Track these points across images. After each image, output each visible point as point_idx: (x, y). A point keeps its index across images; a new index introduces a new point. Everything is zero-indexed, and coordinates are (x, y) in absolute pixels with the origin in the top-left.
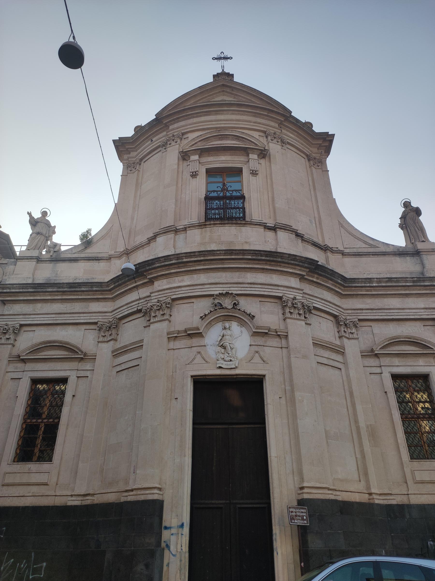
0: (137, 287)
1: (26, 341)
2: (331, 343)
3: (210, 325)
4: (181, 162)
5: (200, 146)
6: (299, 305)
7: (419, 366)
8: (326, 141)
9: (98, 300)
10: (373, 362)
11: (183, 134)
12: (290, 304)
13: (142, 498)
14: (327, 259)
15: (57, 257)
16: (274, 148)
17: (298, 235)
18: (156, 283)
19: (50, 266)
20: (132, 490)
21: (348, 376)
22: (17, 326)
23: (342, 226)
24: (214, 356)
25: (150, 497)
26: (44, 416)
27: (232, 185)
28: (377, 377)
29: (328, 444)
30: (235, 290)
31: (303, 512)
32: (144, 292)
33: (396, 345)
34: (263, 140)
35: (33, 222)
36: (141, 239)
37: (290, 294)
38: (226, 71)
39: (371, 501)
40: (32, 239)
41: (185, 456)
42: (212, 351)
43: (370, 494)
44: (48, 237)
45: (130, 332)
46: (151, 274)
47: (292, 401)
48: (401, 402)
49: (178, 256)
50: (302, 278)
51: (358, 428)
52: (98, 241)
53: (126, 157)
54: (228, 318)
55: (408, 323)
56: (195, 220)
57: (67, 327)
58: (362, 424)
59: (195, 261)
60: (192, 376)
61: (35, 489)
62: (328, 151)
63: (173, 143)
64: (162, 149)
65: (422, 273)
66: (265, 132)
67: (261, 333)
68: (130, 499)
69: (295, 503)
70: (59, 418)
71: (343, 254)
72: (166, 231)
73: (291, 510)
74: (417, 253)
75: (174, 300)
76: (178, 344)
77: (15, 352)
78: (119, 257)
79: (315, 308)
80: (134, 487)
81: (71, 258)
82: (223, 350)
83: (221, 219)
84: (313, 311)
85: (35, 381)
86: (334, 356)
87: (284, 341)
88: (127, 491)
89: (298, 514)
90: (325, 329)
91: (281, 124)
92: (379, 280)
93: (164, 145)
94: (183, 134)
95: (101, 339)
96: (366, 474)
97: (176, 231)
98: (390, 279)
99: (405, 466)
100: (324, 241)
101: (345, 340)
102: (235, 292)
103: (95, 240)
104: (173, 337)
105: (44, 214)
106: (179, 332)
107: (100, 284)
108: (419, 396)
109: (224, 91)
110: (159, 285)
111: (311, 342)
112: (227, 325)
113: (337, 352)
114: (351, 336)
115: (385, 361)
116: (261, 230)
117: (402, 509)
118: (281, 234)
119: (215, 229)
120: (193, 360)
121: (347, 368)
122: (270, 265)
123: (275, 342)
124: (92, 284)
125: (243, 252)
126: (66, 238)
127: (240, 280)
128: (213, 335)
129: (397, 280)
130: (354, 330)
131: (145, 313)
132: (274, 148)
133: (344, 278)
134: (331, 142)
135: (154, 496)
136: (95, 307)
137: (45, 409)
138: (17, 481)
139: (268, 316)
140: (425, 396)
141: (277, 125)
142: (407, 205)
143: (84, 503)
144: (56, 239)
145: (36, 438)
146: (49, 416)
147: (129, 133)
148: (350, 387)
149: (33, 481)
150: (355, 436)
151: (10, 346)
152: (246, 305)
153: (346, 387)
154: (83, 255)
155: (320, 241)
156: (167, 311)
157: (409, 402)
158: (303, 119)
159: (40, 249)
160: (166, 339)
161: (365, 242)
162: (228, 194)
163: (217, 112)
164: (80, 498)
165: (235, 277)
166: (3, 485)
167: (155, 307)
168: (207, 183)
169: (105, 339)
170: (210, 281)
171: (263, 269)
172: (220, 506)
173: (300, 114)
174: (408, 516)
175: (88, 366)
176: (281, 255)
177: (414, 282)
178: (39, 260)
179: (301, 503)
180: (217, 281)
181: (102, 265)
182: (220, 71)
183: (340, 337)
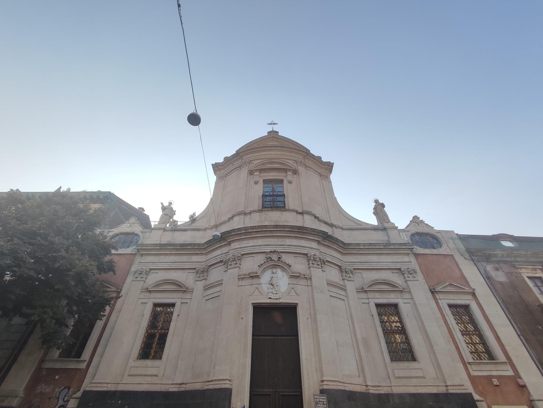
0: (221, 247)
1: (153, 279)
2: (337, 283)
3: (264, 270)
4: (249, 176)
5: (260, 167)
6: (318, 259)
7: (391, 299)
8: (329, 166)
9: (197, 254)
10: (363, 295)
11: (251, 161)
12: (312, 258)
13: (218, 387)
14: (333, 231)
15: (176, 228)
16: (301, 169)
17: (316, 217)
18: (232, 245)
19: (170, 233)
20: (212, 381)
21: (349, 305)
22: (148, 270)
23: (341, 213)
24: (266, 290)
25: (223, 386)
26: (159, 328)
27: (278, 189)
28: (367, 305)
29: (335, 350)
30: (279, 249)
31: (324, 399)
32: (225, 250)
33: (384, 285)
34: (295, 165)
35: (164, 208)
36: (225, 218)
37: (312, 252)
38: (274, 130)
39: (368, 391)
40: (161, 218)
41: (247, 357)
42: (265, 287)
43: (367, 386)
44: (171, 217)
45: (215, 275)
46: (230, 239)
47: (315, 321)
48: (382, 322)
49: (246, 228)
50: (319, 243)
51: (356, 339)
52: (199, 220)
53: (218, 173)
54: (275, 266)
55: (383, 271)
56: (256, 208)
57: (176, 271)
58: (359, 337)
59: (256, 232)
60: (252, 304)
61: (149, 379)
62: (331, 171)
63: (245, 166)
64: (239, 169)
65: (389, 241)
66: (296, 161)
67: (295, 276)
68: (210, 387)
69: (319, 392)
70: (168, 329)
71: (342, 229)
72: (239, 214)
73: (316, 397)
74: (385, 229)
75: (242, 255)
76: (244, 282)
77: (145, 286)
78: (211, 229)
79: (327, 261)
80: (213, 379)
81: (183, 229)
82: (272, 287)
83: (271, 207)
84: (326, 263)
85: (156, 305)
86: (340, 292)
87: (309, 281)
88: (208, 381)
89: (321, 400)
90: (334, 274)
91: (304, 157)
92: (364, 245)
93: (240, 167)
94: (251, 161)
95: (197, 279)
96: (363, 371)
97: (245, 214)
98: (370, 244)
99: (388, 366)
100: (331, 221)
101: (346, 281)
102: (279, 251)
103: (197, 219)
104: (241, 278)
105: (170, 204)
106: (245, 275)
107: (199, 245)
108: (393, 318)
109: (273, 140)
110: (234, 245)
111: (326, 282)
112: (274, 271)
113: (342, 289)
114: (350, 279)
115: (371, 295)
116: (295, 214)
117: (388, 396)
118: (306, 216)
119: (268, 213)
120: (254, 292)
121: (348, 299)
122: (300, 234)
123: (303, 282)
124: (194, 245)
125: (284, 226)
126: (181, 217)
127: (282, 243)
128: (266, 277)
129: (375, 244)
130: (351, 275)
131: (225, 263)
132: (301, 169)
133: (344, 243)
134: (332, 166)
135: (226, 385)
136: (195, 258)
137: (160, 323)
138: (138, 373)
139: (299, 265)
140: (397, 318)
141: (302, 157)
142: (376, 201)
143: (180, 390)
144: (175, 218)
145: (153, 343)
146: (162, 328)
147: (221, 160)
148: (351, 312)
149: (148, 373)
150: (355, 345)
151: (143, 282)
152: (286, 258)
153: (348, 312)
154: (190, 227)
155: (328, 221)
156: (238, 262)
157: (387, 322)
158: (316, 154)
159: (166, 224)
160: (237, 279)
161: (355, 222)
162: (275, 194)
163: (269, 150)
164: (178, 386)
165: (279, 241)
166: (129, 376)
167: (231, 259)
168: (264, 187)
169: (200, 279)
170: (264, 244)
171: (296, 237)
172: (270, 393)
173: (315, 152)
174: (392, 403)
175: (188, 296)
176: (306, 229)
177: (384, 246)
178: (164, 230)
179: (322, 392)
180: (269, 243)
181: (201, 233)
182: (271, 130)
183: (343, 280)
